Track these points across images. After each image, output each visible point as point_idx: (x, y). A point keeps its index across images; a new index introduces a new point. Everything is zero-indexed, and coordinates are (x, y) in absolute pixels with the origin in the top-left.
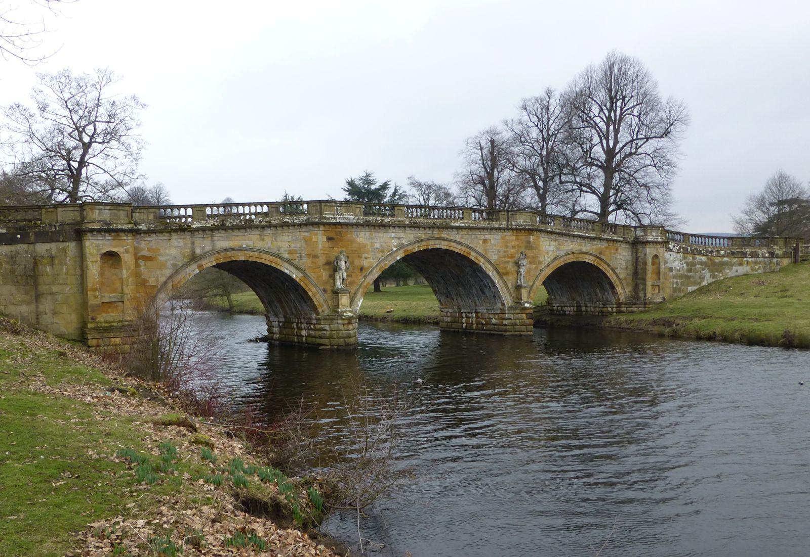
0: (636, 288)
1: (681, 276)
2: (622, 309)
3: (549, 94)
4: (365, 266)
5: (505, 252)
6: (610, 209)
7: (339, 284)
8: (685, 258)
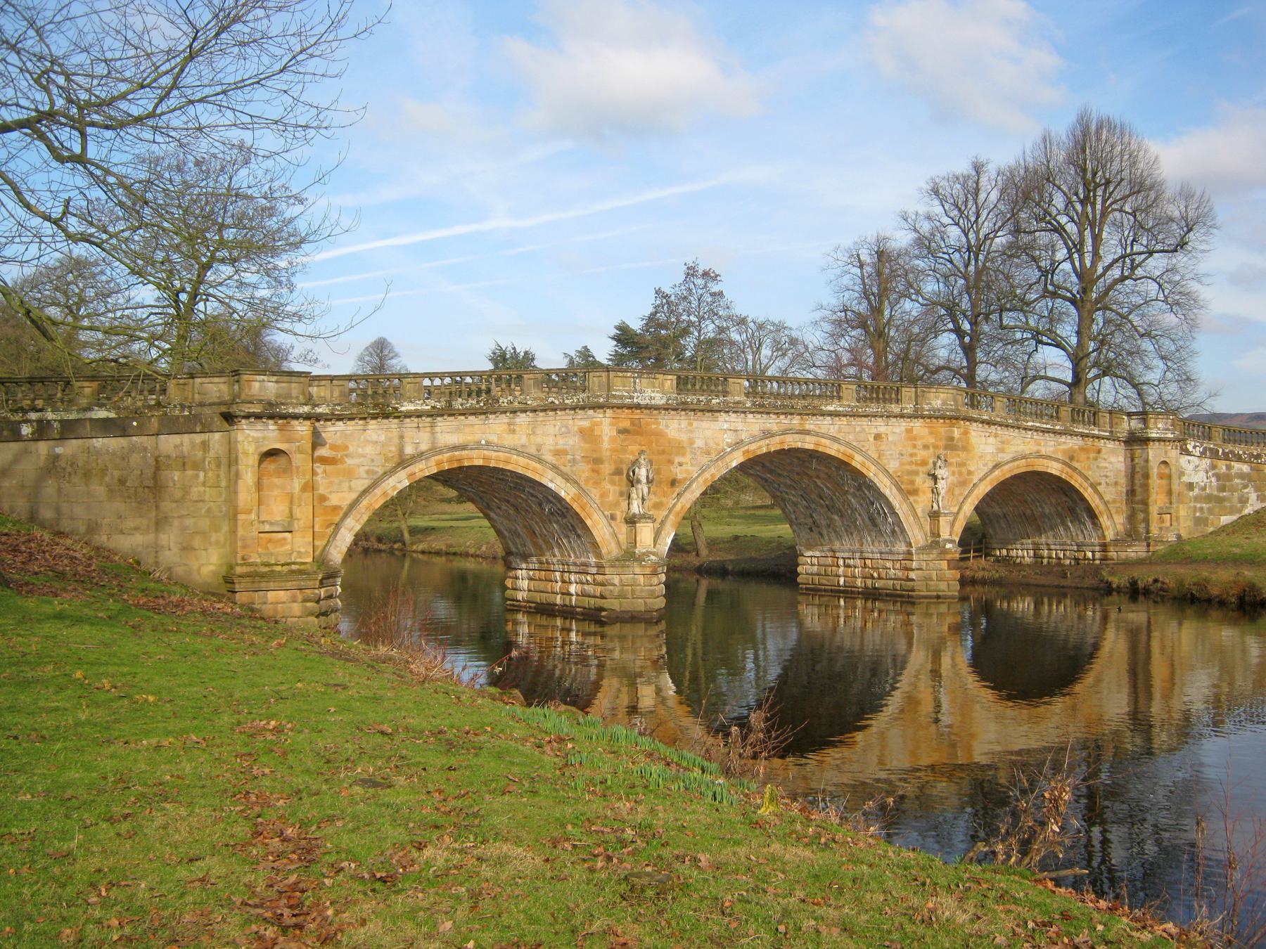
0: (1131, 518)
1: (1209, 498)
2: (1110, 554)
3: (978, 168)
4: (680, 476)
5: (912, 455)
6: (1090, 375)
8: (1213, 467)
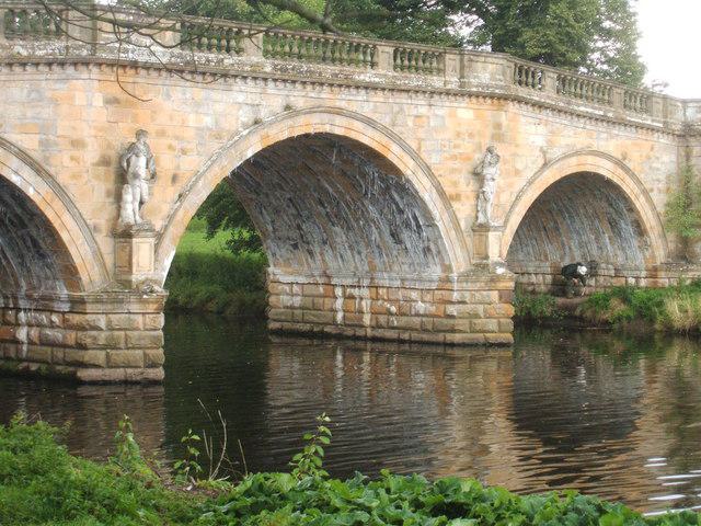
2: (661, 281)
7: (130, 212)
